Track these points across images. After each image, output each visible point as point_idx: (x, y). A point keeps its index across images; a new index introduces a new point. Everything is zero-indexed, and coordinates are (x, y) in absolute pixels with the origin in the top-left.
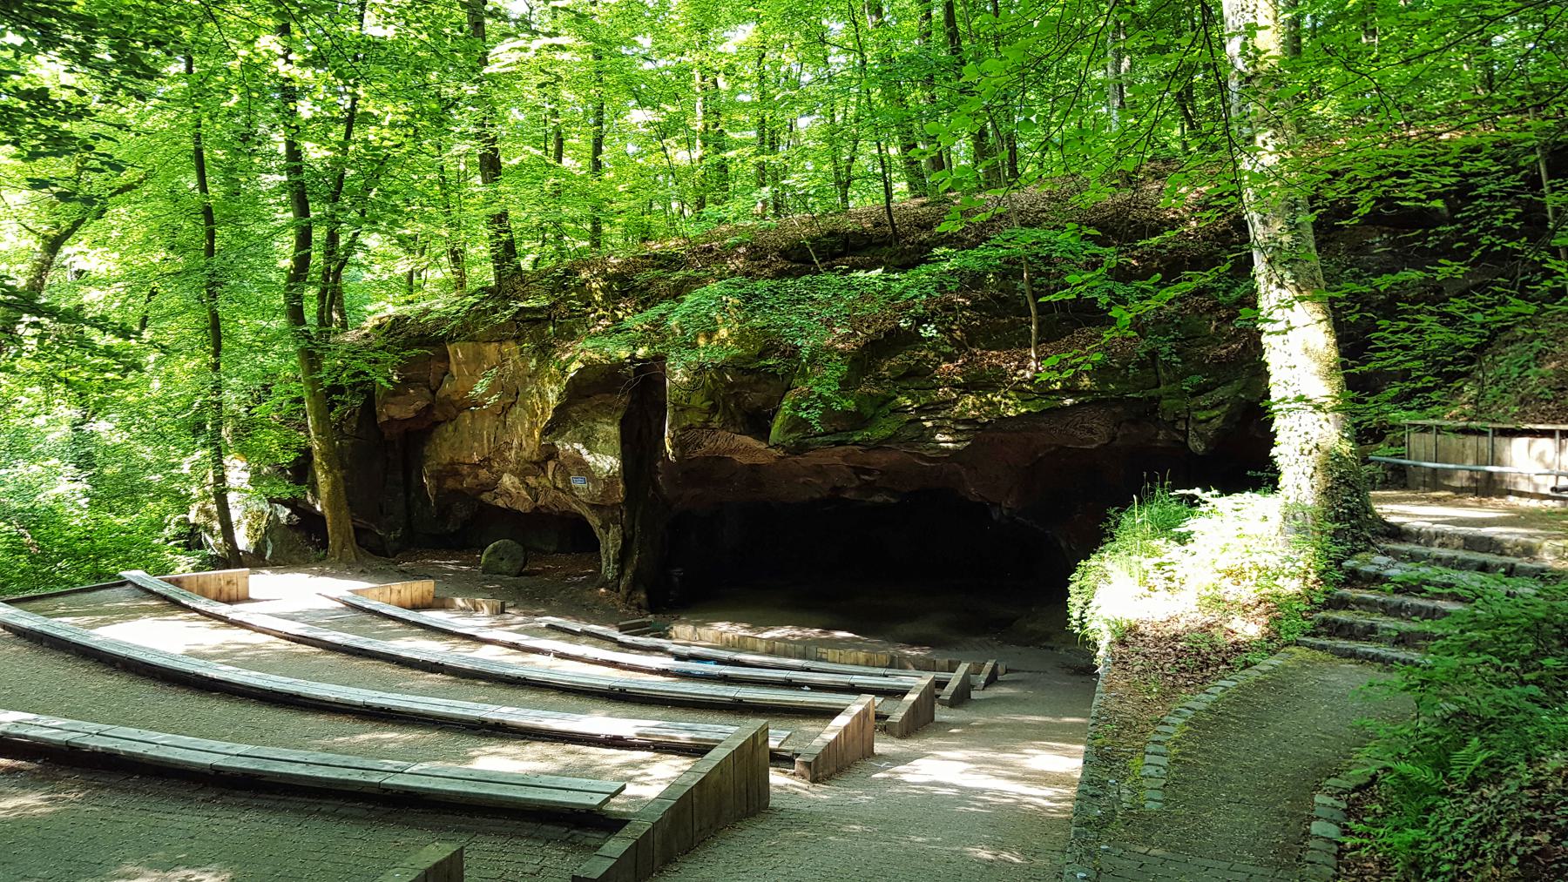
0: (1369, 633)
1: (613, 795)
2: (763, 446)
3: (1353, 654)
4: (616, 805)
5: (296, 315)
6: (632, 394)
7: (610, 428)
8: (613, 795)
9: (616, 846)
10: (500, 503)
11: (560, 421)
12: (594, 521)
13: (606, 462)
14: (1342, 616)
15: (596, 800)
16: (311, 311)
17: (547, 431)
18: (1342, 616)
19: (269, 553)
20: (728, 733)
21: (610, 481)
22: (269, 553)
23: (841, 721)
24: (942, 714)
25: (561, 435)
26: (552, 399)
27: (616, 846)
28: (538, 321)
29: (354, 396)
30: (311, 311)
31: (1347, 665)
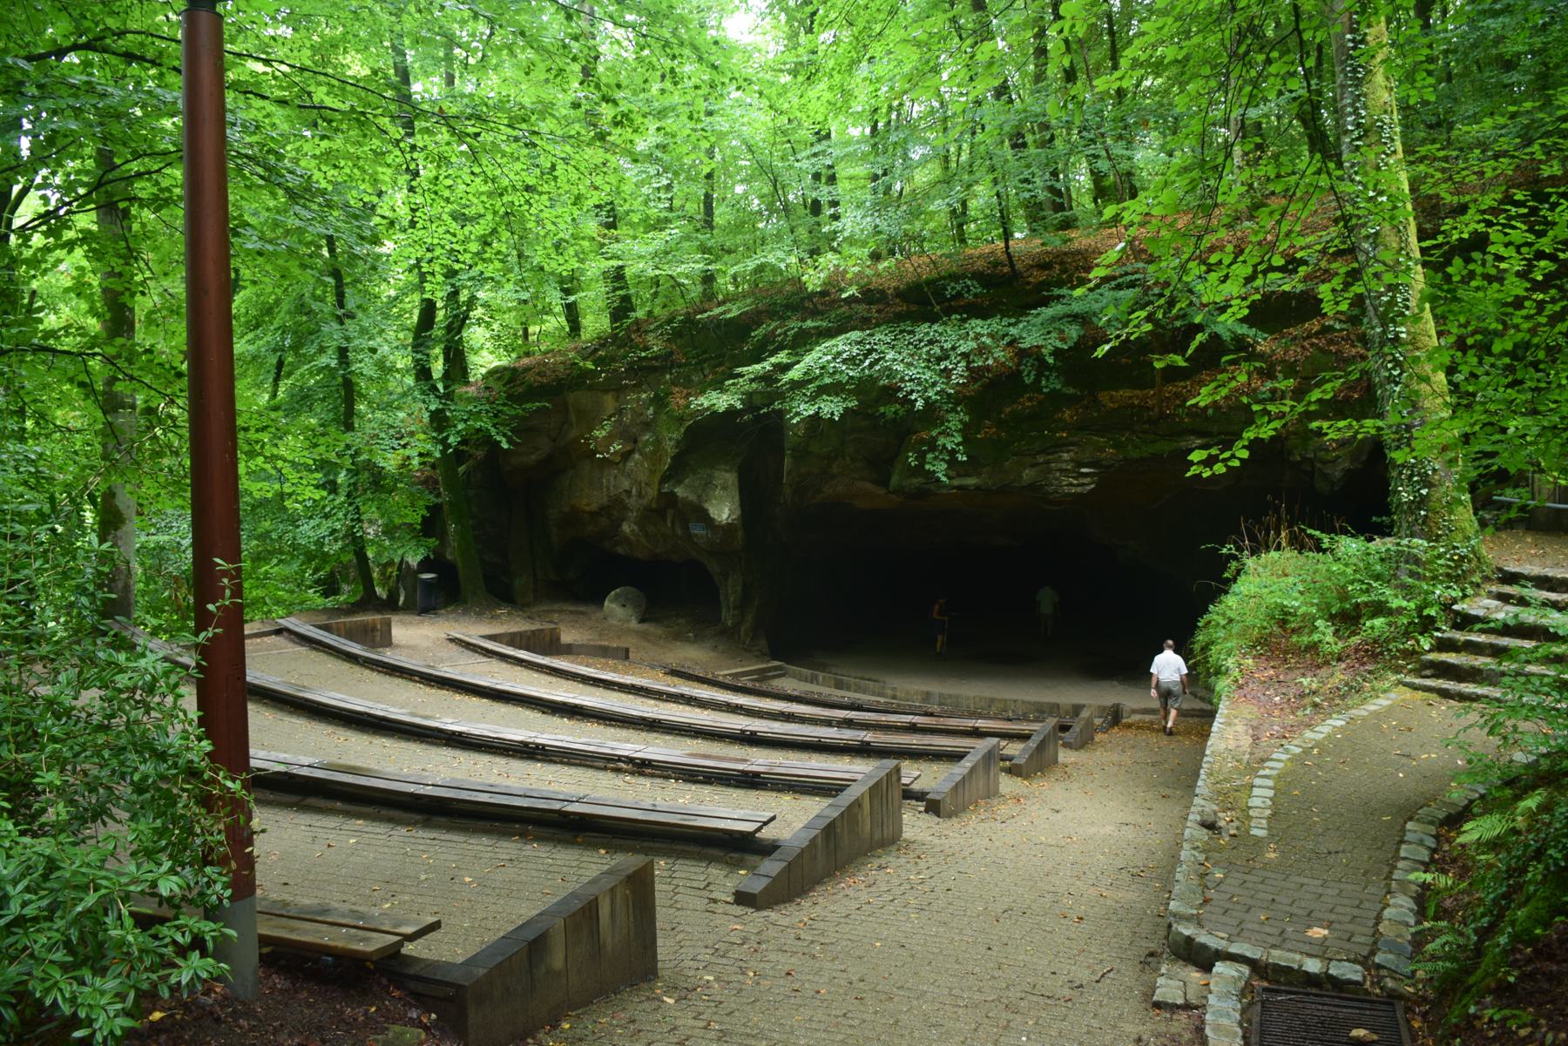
0: (1472, 675)
1: (765, 823)
2: (882, 491)
3: (1462, 697)
4: (766, 834)
5: (423, 373)
6: (752, 438)
7: (727, 475)
8: (765, 823)
9: (772, 866)
10: (620, 550)
11: (678, 469)
12: (714, 567)
13: (723, 511)
14: (1451, 658)
15: (748, 827)
16: (438, 368)
17: (665, 479)
18: (1451, 658)
19: (402, 599)
20: (860, 770)
21: (729, 528)
22: (402, 599)
23: (967, 763)
24: (1064, 756)
25: (680, 482)
26: (670, 447)
27: (772, 866)
28: (654, 369)
29: (160, 295)
30: (438, 368)
31: (1444, 706)
